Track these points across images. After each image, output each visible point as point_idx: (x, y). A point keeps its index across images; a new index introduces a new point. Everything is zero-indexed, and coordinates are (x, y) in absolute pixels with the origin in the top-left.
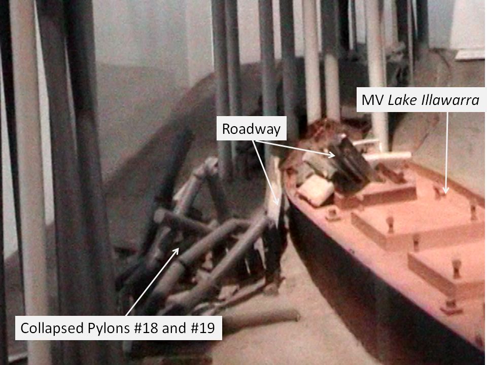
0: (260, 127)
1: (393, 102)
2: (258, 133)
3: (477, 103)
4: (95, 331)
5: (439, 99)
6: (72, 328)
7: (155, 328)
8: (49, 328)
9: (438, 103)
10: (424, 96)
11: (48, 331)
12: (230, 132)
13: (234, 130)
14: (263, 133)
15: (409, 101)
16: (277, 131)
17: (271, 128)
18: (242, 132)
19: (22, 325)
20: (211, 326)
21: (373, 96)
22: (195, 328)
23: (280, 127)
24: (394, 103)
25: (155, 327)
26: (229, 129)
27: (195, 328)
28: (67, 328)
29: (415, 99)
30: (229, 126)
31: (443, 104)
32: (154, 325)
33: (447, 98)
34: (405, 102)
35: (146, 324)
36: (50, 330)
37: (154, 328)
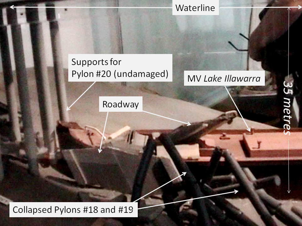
0: (126, 103)
1: (207, 80)
2: (125, 107)
3: (259, 81)
4: (59, 211)
5: (235, 78)
6: (44, 209)
7: (96, 210)
8: (135, 74)
9: (235, 81)
10: (226, 76)
11: (30, 212)
12: (107, 106)
13: (110, 105)
14: (128, 107)
15: (217, 79)
16: (137, 106)
17: (133, 104)
18: (115, 106)
19: (14, 208)
20: (131, 208)
21: (194, 76)
22: (121, 210)
23: (138, 103)
24: (208, 81)
25: (96, 209)
26: (107, 104)
27: (121, 210)
28: (41, 210)
29: (220, 78)
30: (106, 103)
31: (238, 81)
32: (96, 208)
33: (240, 78)
34: (214, 80)
35: (91, 207)
36: (31, 211)
37: (95, 210)
